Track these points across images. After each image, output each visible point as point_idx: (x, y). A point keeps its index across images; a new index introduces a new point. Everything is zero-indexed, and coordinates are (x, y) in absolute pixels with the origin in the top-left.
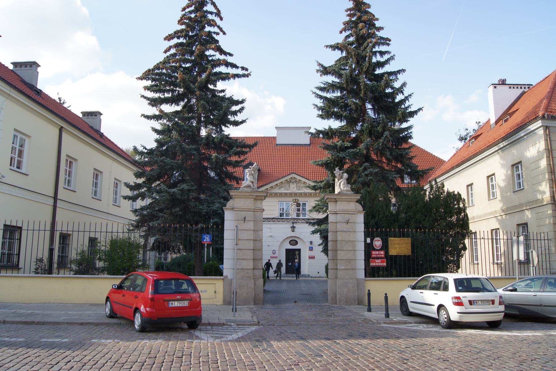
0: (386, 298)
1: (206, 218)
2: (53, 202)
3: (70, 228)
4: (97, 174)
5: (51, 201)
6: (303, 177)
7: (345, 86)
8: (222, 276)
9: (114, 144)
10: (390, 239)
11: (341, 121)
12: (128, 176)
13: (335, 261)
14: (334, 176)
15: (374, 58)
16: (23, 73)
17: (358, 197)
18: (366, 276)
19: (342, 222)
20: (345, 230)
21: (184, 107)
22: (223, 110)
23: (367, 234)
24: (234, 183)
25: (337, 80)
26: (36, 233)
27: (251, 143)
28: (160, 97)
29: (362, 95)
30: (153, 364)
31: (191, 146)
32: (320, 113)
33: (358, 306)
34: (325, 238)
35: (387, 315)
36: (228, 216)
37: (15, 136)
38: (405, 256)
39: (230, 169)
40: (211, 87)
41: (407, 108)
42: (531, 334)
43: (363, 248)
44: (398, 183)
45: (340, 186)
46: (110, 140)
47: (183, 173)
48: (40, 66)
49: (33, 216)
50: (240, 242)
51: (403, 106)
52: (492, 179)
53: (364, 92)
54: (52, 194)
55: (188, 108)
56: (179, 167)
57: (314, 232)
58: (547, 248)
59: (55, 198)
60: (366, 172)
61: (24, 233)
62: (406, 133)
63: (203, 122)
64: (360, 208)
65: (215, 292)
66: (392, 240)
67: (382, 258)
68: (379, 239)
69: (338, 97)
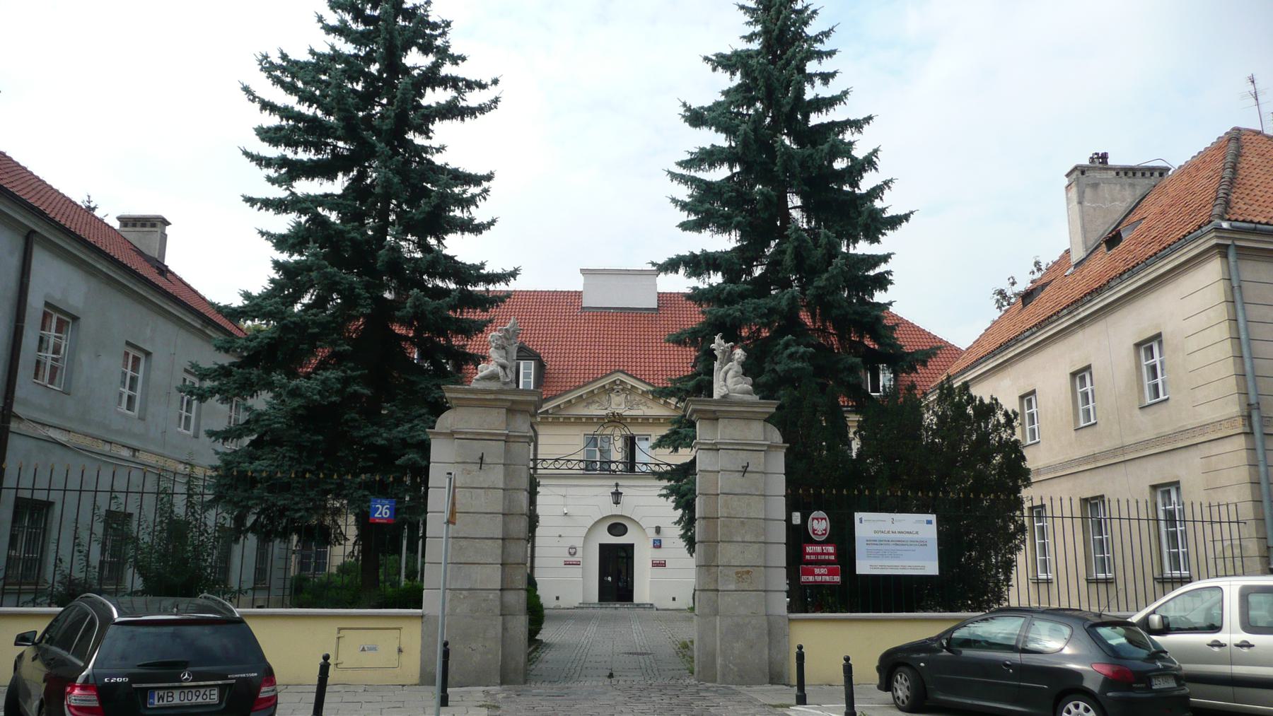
0: (848, 669)
1: (385, 457)
3: (42, 482)
6: (640, 380)
9: (200, 296)
13: (714, 569)
14: (710, 356)
15: (808, 87)
20: (738, 491)
22: (439, 199)
33: (768, 687)
36: (442, 455)
37: (127, 354)
43: (783, 538)
50: (140, 474)
53: (781, 165)
58: (1236, 542)
60: (788, 351)
63: (393, 223)
64: (776, 437)
68: (822, 514)
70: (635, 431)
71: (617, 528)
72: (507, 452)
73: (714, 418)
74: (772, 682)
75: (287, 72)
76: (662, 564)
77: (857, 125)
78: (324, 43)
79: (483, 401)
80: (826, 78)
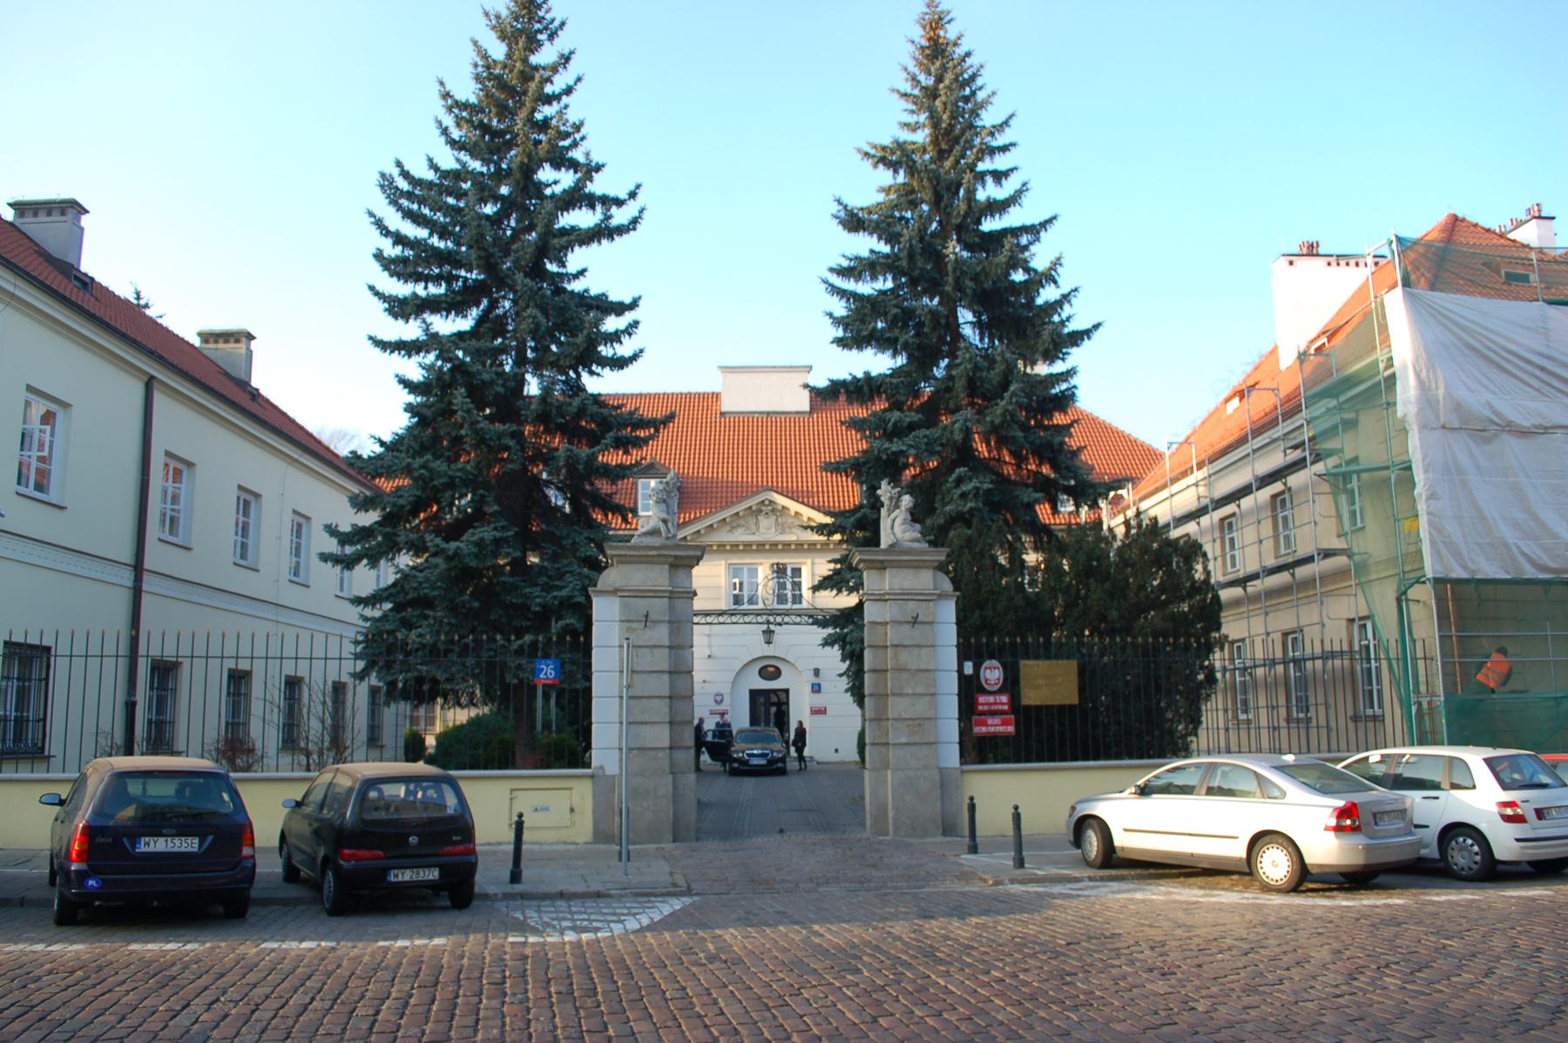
0: (1017, 818)
2: (132, 577)
3: (245, 651)
4: (248, 500)
5: (127, 577)
7: (904, 263)
8: (589, 766)
10: (1023, 663)
11: (894, 356)
12: (336, 508)
14: (876, 505)
16: (45, 231)
17: (940, 555)
18: (964, 757)
19: (900, 623)
21: (480, 321)
22: (580, 328)
23: (966, 651)
24: (616, 521)
25: (885, 248)
26: (94, 663)
27: (658, 413)
28: (415, 295)
29: (948, 288)
30: (433, 1002)
31: (499, 427)
32: (840, 333)
34: (854, 656)
35: (1020, 863)
36: (606, 615)
37: (28, 404)
38: (1061, 708)
39: (604, 486)
40: (552, 267)
41: (1062, 323)
42: (1380, 902)
44: (1043, 512)
45: (896, 526)
46: (276, 407)
47: (483, 496)
48: (87, 212)
49: (70, 613)
51: (1056, 318)
52: (1283, 501)
53: (952, 289)
54: (127, 555)
55: (489, 325)
56: (470, 483)
57: (828, 642)
59: (138, 567)
61: (60, 667)
62: (1064, 386)
64: (947, 586)
65: (572, 810)
66: (1028, 667)
67: (1003, 712)
68: (995, 663)
69: (883, 293)
70: (789, 560)
71: (770, 672)
72: (672, 609)
73: (882, 566)
74: (945, 833)
75: (411, 194)
76: (819, 711)
77: (1034, 230)
78: (448, 160)
79: (645, 558)
80: (999, 176)
